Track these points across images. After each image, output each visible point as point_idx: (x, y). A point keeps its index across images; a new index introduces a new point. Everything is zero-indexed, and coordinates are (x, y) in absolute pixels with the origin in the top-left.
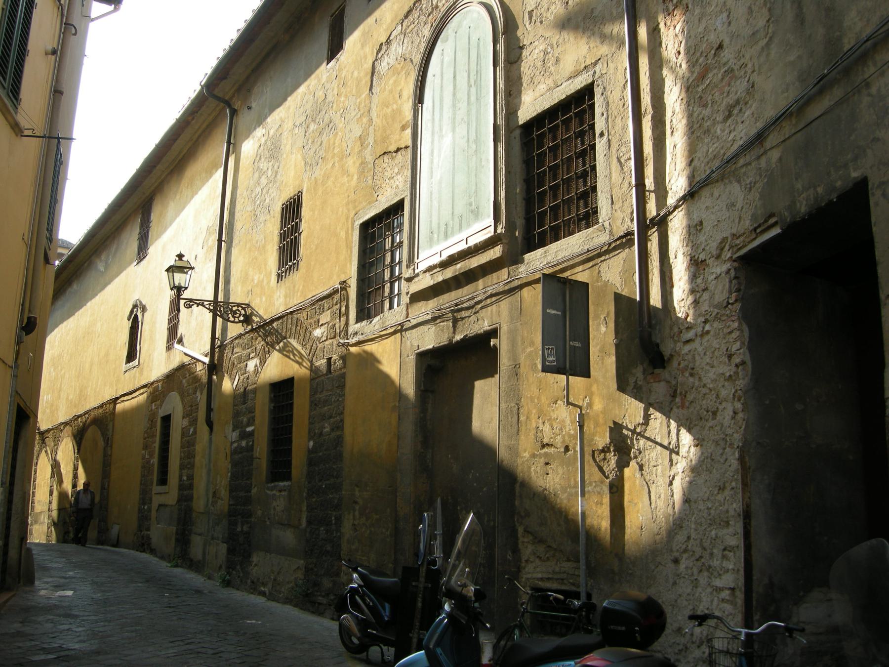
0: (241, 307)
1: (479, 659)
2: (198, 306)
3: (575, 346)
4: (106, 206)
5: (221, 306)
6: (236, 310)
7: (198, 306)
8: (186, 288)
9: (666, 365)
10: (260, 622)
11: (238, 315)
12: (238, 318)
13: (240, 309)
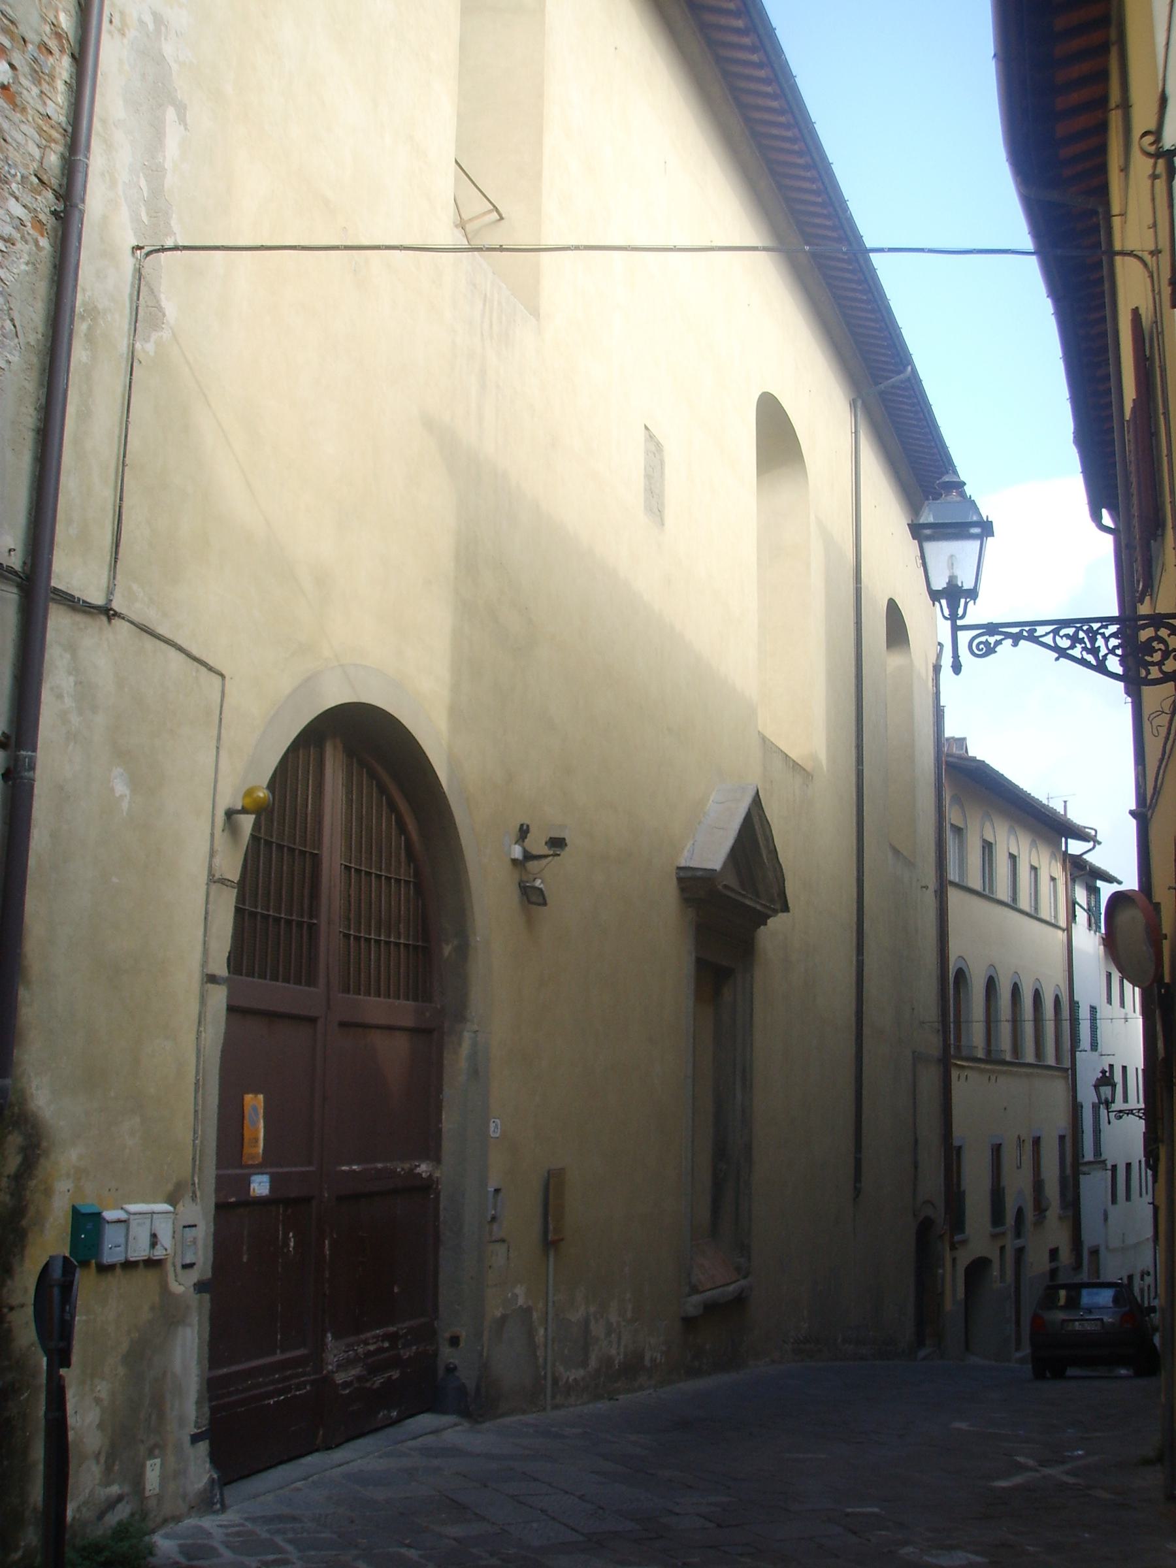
2: (1015, 644)
3: (1109, 359)
4: (1001, 772)
5: (1096, 632)
6: (1151, 640)
7: (1015, 644)
8: (972, 594)
9: (52, 249)
10: (280, 1270)
11: (1157, 657)
12: (1160, 664)
13: (1163, 633)
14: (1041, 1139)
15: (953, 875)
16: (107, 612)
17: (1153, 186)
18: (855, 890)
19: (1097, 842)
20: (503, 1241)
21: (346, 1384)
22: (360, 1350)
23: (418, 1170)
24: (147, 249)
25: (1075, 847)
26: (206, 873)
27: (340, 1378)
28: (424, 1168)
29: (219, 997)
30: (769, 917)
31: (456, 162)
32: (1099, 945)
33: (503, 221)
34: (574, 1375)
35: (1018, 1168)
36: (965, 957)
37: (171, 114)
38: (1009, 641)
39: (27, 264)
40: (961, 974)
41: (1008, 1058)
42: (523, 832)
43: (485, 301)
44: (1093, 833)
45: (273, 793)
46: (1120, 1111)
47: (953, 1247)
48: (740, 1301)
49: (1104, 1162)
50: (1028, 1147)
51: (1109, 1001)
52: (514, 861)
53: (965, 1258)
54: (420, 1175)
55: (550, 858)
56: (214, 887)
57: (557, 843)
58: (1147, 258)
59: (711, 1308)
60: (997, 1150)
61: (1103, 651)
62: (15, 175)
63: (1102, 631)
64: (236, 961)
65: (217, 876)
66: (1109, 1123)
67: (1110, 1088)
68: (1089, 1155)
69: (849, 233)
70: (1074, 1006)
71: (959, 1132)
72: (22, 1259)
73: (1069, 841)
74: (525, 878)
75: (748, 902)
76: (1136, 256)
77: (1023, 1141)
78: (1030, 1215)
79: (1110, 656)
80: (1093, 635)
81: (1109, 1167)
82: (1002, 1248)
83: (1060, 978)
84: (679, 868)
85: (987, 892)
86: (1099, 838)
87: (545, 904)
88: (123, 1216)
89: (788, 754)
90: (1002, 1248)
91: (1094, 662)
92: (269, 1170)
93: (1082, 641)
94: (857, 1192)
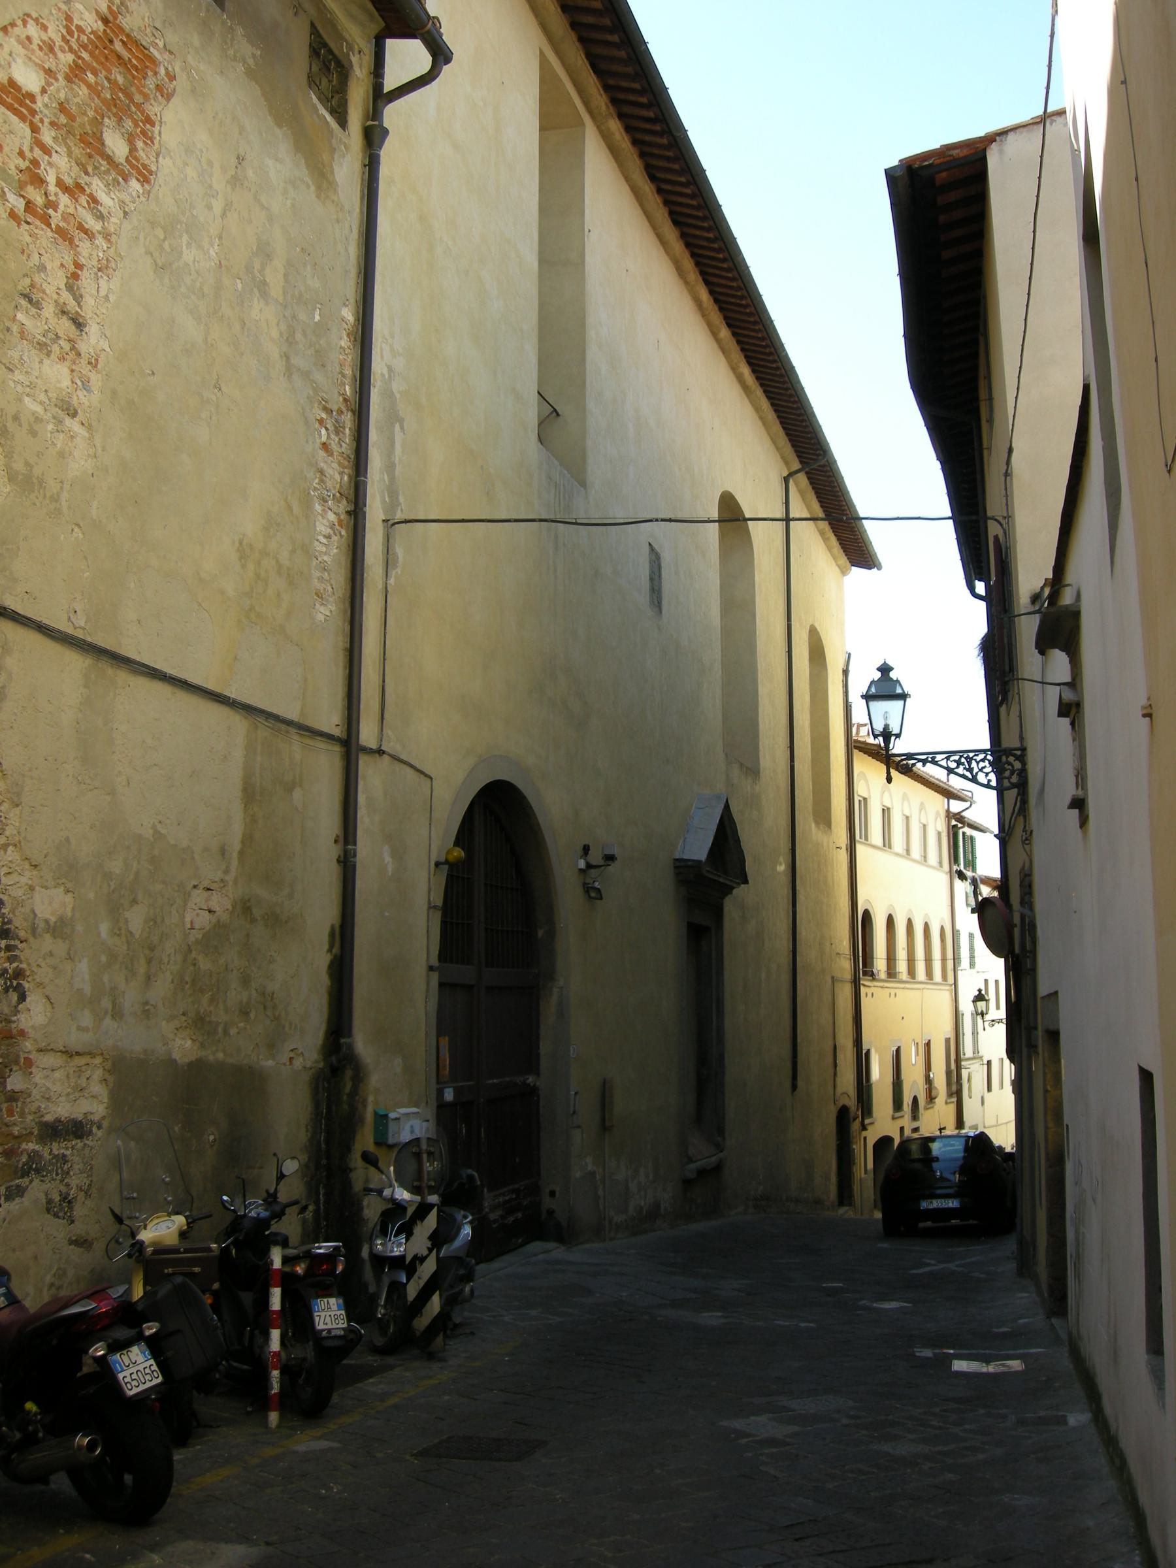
0: (1014, 755)
1: (1016, 1373)
5: (971, 759)
8: (898, 736)
12: (1009, 778)
13: (1011, 759)
16: (380, 752)
17: (1006, 480)
20: (579, 1127)
21: (495, 1221)
22: (501, 1200)
23: (528, 1081)
26: (426, 904)
27: (492, 1216)
28: (530, 1080)
29: (435, 977)
30: (734, 888)
31: (539, 392)
34: (619, 1218)
36: (441, 20)
37: (397, 426)
38: (921, 764)
39: (337, 548)
40: (867, 915)
42: (586, 849)
43: (556, 486)
45: (469, 851)
46: (993, 1021)
48: (718, 1168)
49: (981, 1058)
52: (581, 870)
54: (529, 1084)
55: (603, 868)
56: (431, 910)
57: (610, 858)
58: (1003, 522)
59: (702, 1173)
61: (976, 770)
62: (330, 496)
63: (975, 758)
64: (442, 957)
65: (432, 905)
66: (984, 1029)
67: (985, 1002)
68: (968, 1051)
70: (955, 934)
72: (354, 1143)
73: (951, 801)
74: (587, 881)
75: (722, 880)
76: (996, 520)
79: (980, 773)
80: (969, 760)
84: (676, 860)
87: (601, 898)
88: (398, 1116)
91: (970, 777)
92: (454, 1085)
93: (963, 764)
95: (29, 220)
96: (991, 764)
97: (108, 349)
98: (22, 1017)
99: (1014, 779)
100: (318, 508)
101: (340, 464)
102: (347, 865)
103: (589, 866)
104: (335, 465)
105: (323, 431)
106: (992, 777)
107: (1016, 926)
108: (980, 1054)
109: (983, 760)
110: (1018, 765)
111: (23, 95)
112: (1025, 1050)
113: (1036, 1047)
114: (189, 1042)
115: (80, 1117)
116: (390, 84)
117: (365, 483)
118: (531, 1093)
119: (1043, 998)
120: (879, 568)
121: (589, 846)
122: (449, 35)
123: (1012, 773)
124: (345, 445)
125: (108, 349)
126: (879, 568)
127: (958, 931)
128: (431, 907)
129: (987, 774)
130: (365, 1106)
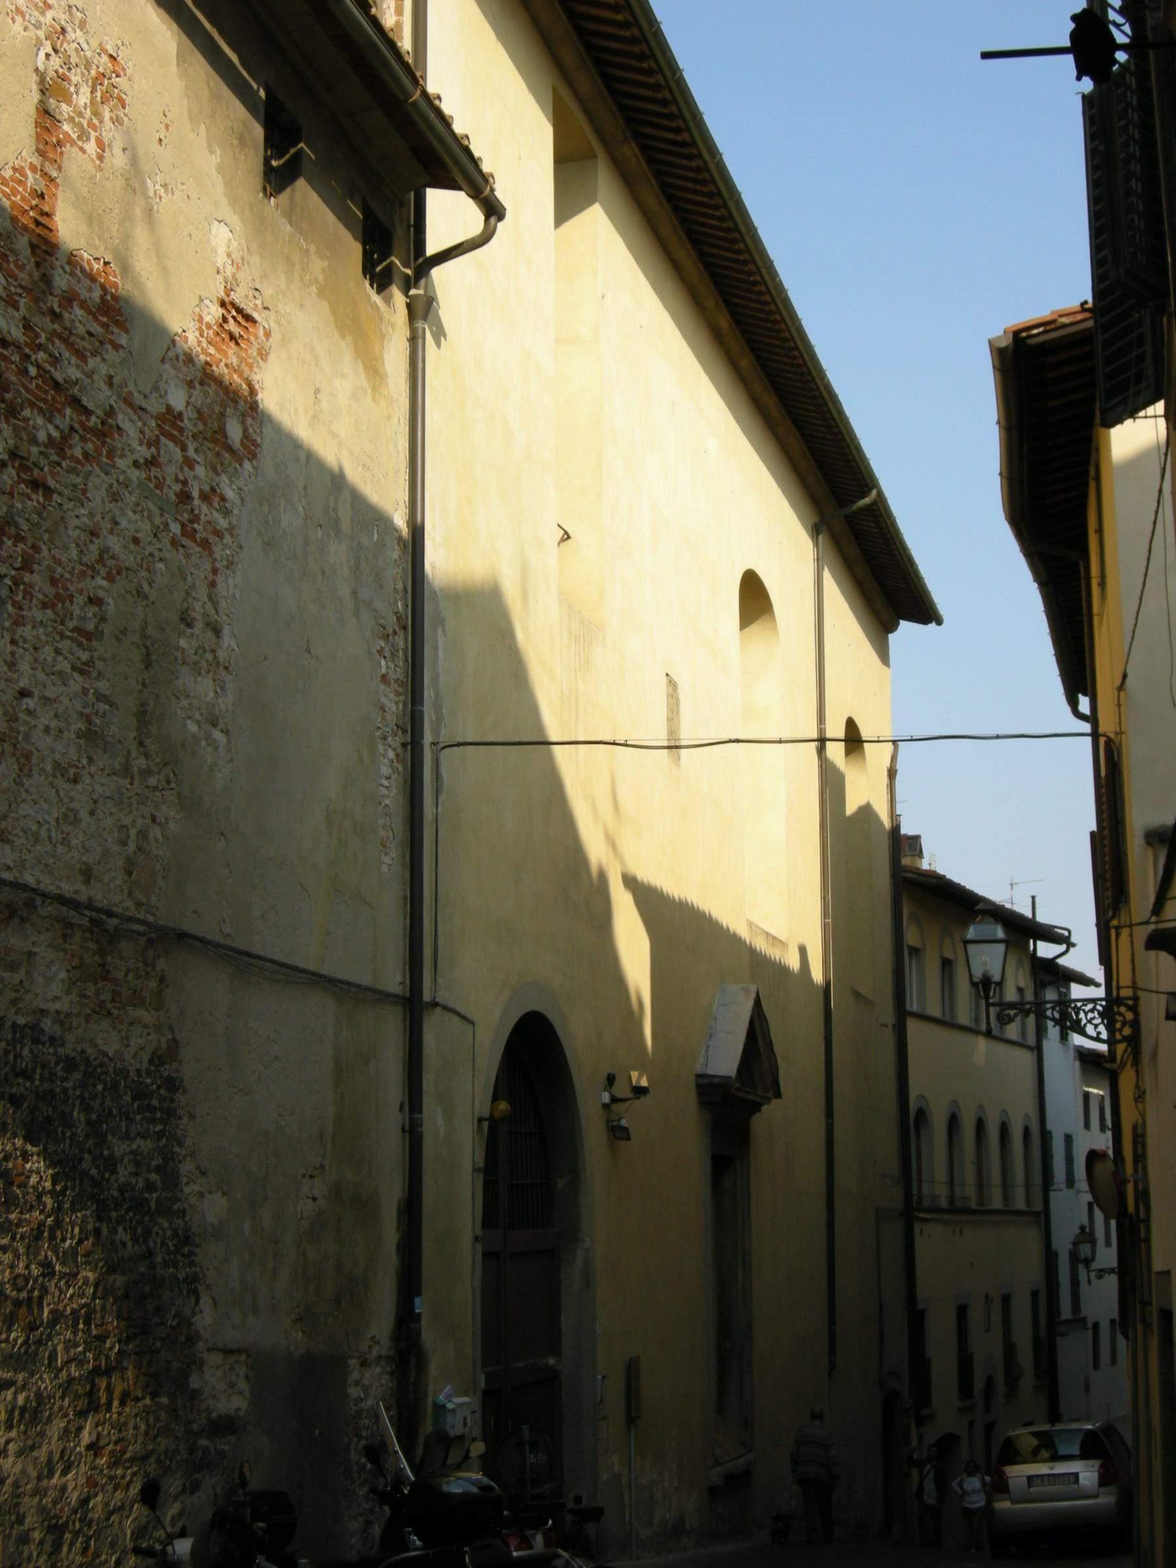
12: (1120, 1030)
13: (1123, 1009)
14: (251, 161)
15: (913, 1005)
18: (823, 1049)
19: (1070, 945)
20: (605, 1418)
24: (442, 745)
25: (1046, 950)
30: (762, 1105)
32: (1075, 1059)
33: (569, 541)
35: (987, 1331)
40: (921, 1113)
41: (974, 1206)
42: (611, 1080)
44: (1066, 933)
47: (920, 1423)
49: (1084, 1320)
50: (997, 1309)
51: (1087, 1125)
53: (933, 1433)
60: (962, 1312)
68: (1066, 1313)
69: (808, 360)
70: (1046, 1136)
71: (923, 1291)
77: (992, 1300)
78: (1001, 1387)
79: (1088, 1025)
81: (1090, 1325)
82: (971, 1424)
83: (1032, 1110)
84: (698, 1076)
85: (947, 1019)
86: (1073, 940)
87: (629, 1139)
89: (768, 931)
90: (971, 1424)
94: (832, 1366)
95: (184, 543)
96: (1101, 1014)
97: (236, 648)
98: (197, 1319)
99: (1127, 1031)
100: (381, 748)
101: (398, 694)
102: (413, 1135)
103: (614, 1100)
104: (392, 696)
105: (383, 662)
106: (1102, 1028)
107: (1129, 1181)
108: (1083, 1315)
109: (1092, 1011)
110: (1129, 1016)
111: (174, 417)
112: (1140, 1327)
113: (1151, 1325)
114: (301, 1334)
115: (231, 1412)
116: (432, 248)
117: (422, 712)
118: (552, 1378)
119: (1157, 1273)
120: (939, 622)
121: (614, 1075)
122: (502, 192)
123: (1124, 1024)
124: (397, 670)
125: (236, 648)
126: (939, 622)
127: (1050, 1132)
128: (476, 1170)
129: (1096, 1026)
130: (426, 1396)
